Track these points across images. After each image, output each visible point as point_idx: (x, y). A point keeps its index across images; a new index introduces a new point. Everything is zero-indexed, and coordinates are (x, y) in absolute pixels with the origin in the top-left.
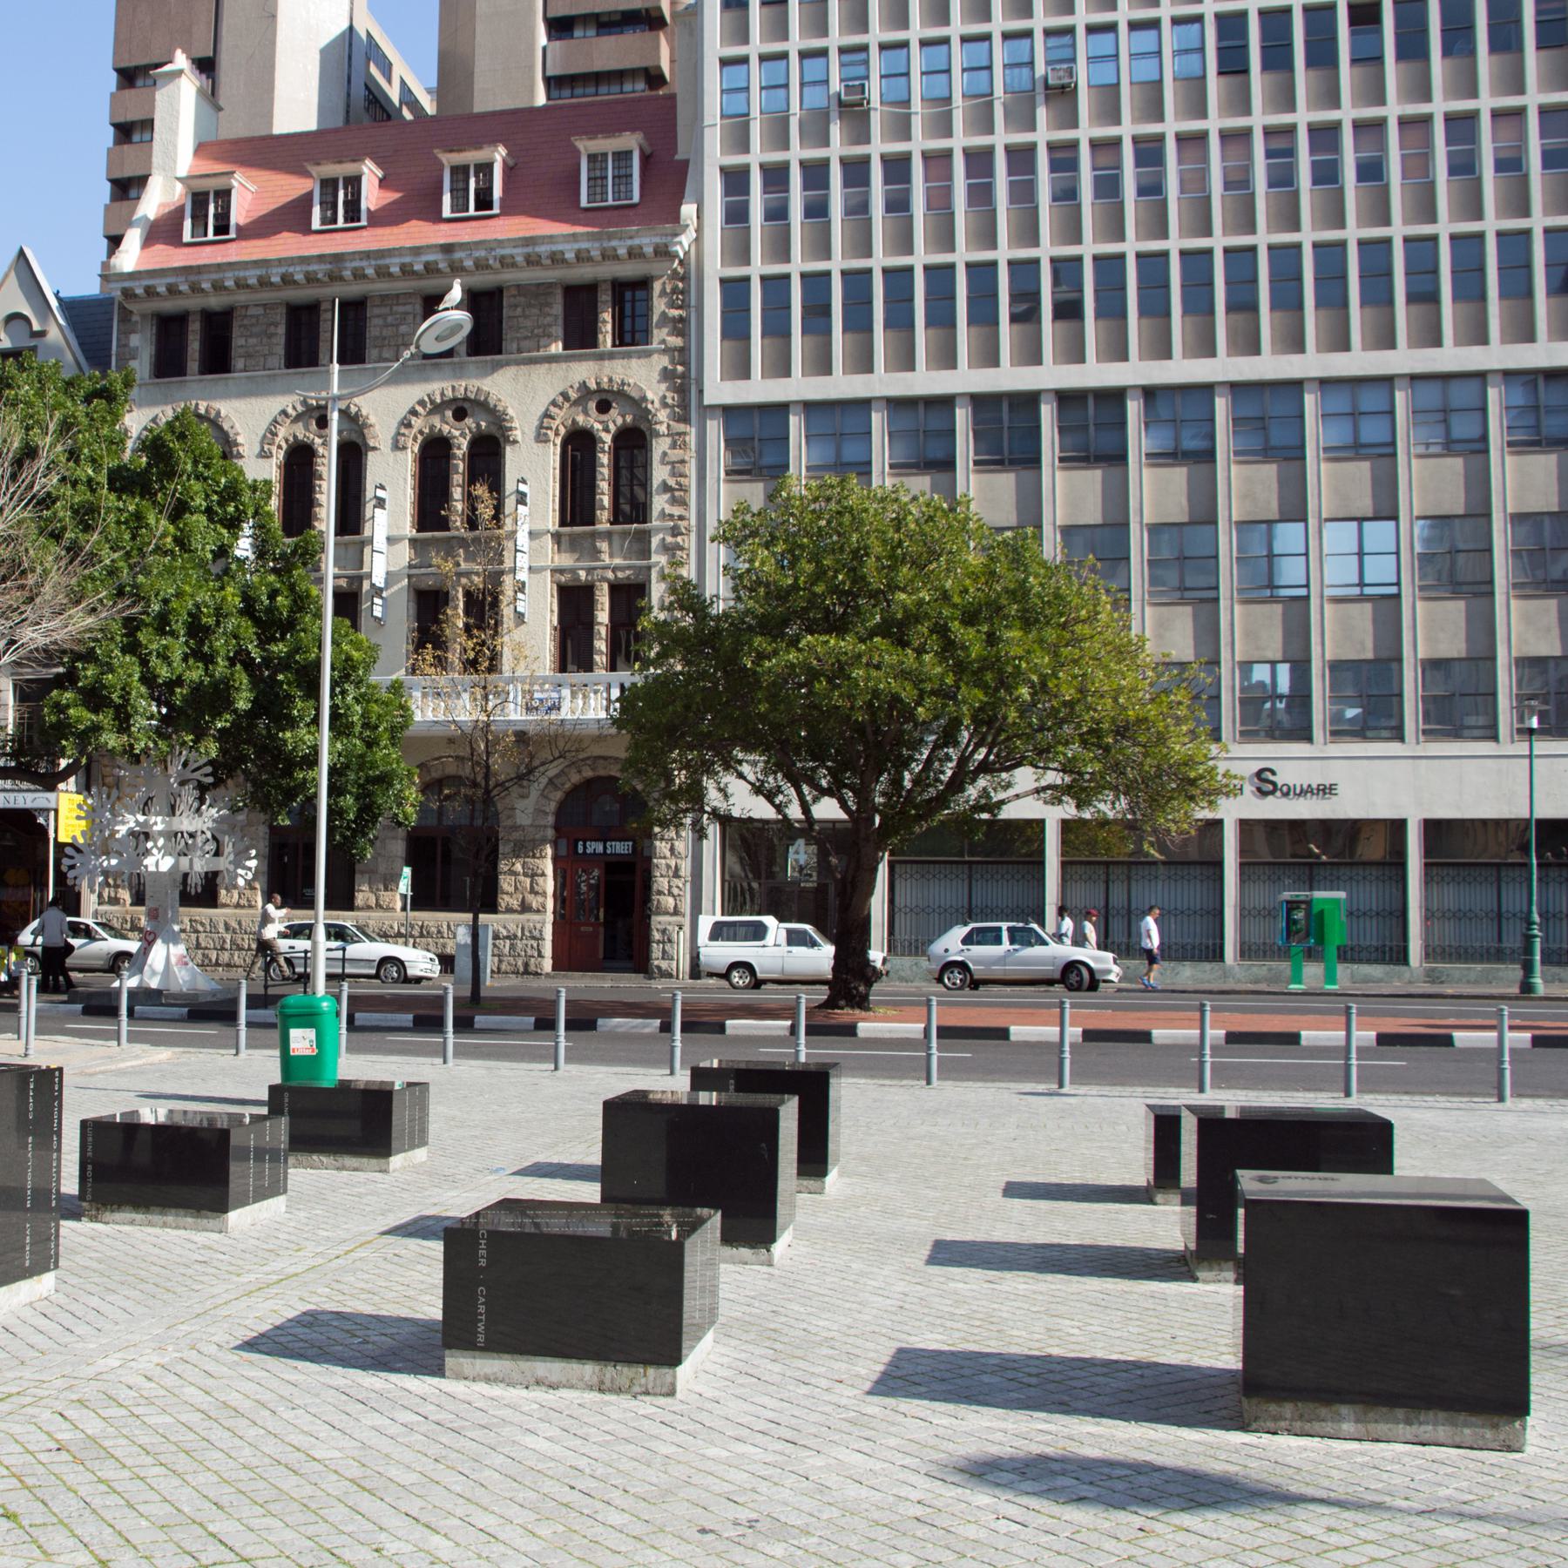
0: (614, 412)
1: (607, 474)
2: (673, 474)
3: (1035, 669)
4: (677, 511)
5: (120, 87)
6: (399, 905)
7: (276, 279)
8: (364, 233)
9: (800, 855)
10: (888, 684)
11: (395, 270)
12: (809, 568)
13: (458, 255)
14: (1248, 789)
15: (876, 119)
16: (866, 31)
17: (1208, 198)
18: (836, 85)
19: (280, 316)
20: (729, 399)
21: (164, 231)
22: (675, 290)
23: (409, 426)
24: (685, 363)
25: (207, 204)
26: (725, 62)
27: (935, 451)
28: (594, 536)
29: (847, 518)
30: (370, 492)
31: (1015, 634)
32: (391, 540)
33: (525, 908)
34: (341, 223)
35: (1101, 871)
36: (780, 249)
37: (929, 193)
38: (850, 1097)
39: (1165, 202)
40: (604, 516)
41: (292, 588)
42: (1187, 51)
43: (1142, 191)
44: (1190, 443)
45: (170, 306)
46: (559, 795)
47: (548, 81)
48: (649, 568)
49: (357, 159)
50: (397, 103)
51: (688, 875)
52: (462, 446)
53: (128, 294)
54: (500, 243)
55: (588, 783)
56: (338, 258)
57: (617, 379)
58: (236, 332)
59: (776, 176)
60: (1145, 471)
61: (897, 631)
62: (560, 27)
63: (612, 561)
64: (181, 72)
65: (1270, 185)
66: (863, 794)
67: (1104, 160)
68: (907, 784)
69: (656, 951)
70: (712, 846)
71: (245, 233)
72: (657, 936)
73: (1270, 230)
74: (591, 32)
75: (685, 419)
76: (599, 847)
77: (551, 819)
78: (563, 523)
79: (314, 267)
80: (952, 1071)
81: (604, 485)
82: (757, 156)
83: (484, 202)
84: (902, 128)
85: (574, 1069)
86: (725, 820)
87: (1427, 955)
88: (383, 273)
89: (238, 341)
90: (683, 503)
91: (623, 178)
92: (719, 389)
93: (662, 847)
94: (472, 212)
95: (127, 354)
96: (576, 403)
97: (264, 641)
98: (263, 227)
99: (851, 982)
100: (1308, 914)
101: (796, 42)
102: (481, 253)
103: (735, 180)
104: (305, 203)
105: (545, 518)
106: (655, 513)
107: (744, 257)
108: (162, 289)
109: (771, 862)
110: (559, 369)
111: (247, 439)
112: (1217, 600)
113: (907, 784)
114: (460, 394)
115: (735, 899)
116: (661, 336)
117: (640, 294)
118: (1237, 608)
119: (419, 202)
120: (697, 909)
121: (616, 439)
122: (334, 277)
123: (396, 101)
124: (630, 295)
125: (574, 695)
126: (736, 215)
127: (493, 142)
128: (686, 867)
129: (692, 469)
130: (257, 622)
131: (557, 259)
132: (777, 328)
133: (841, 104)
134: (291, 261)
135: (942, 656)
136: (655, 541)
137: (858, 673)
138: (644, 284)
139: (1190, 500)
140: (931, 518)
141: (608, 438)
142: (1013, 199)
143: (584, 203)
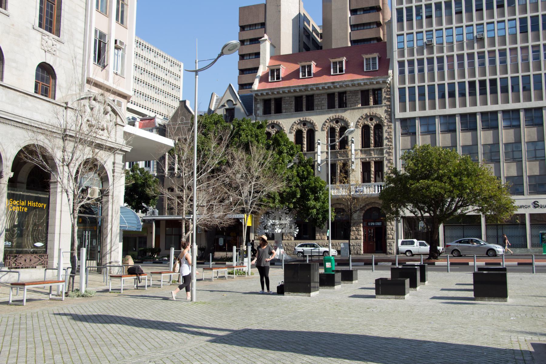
0: (374, 121)
1: (373, 136)
2: (388, 135)
3: (470, 186)
4: (390, 144)
5: (241, 31)
6: (326, 239)
7: (292, 91)
8: (312, 79)
9: (421, 224)
10: (438, 190)
11: (321, 88)
12: (421, 165)
13: (336, 84)
14: (532, 206)
15: (435, 48)
16: (432, 27)
17: (518, 64)
18: (425, 40)
19: (293, 99)
20: (401, 117)
21: (264, 79)
22: (387, 91)
23: (325, 125)
24: (390, 108)
25: (274, 72)
26: (398, 35)
27: (451, 128)
28: (370, 150)
29: (429, 155)
30: (316, 141)
31: (466, 179)
32: (322, 152)
33: (356, 239)
34: (307, 76)
35: (496, 227)
36: (412, 80)
37: (448, 65)
38: (429, 274)
39: (507, 65)
40: (372, 145)
41: (307, 170)
42: (512, 28)
43: (501, 63)
44: (515, 123)
45: (267, 97)
46: (363, 212)
47: (351, 26)
48: (383, 157)
49: (310, 61)
50: (311, 31)
51: (395, 231)
52: (338, 129)
53: (257, 95)
54: (345, 81)
55: (370, 209)
56: (307, 86)
57: (374, 113)
58: (283, 103)
59: (411, 63)
60: (503, 131)
61: (440, 178)
62: (354, 12)
63: (375, 156)
64: (266, 40)
65: (534, 60)
66: (435, 212)
67: (492, 55)
68: (444, 210)
69: (388, 248)
70: (401, 225)
71: (284, 79)
72: (388, 244)
73: (533, 71)
74: (362, 13)
75: (391, 122)
76: (374, 224)
77: (362, 217)
78: (362, 147)
79: (301, 88)
80: (452, 270)
81: (372, 138)
82: (406, 58)
83: (341, 70)
84: (441, 50)
85: (376, 271)
86: (403, 217)
87: (532, 246)
88: (318, 89)
89: (283, 106)
90: (391, 142)
91: (374, 64)
92: (399, 115)
93: (388, 223)
94: (338, 73)
95: (257, 109)
96: (365, 119)
97: (301, 181)
98: (288, 78)
99: (434, 254)
100: (165, 260)
101: (415, 30)
102: (341, 84)
103: (401, 64)
104: (297, 72)
105: (358, 146)
106: (384, 145)
107: (404, 83)
108: (265, 94)
109: (415, 226)
110: (360, 111)
111: (286, 130)
112: (522, 161)
113: (444, 210)
114: (337, 117)
115: (406, 236)
116: (384, 102)
117: (379, 92)
118: (527, 163)
119: (326, 71)
120: (397, 238)
121: (374, 127)
122: (306, 90)
123: (311, 31)
124: (377, 93)
125: (367, 188)
126: (402, 72)
127: (343, 56)
128: (394, 228)
129: (393, 134)
130: (300, 178)
131: (359, 85)
132: (412, 100)
133: (426, 45)
134: (296, 87)
135: (450, 184)
136: (385, 151)
137: (432, 188)
138: (380, 89)
139: (515, 137)
140: (447, 154)
141: (372, 127)
142: (469, 66)
143: (365, 70)
